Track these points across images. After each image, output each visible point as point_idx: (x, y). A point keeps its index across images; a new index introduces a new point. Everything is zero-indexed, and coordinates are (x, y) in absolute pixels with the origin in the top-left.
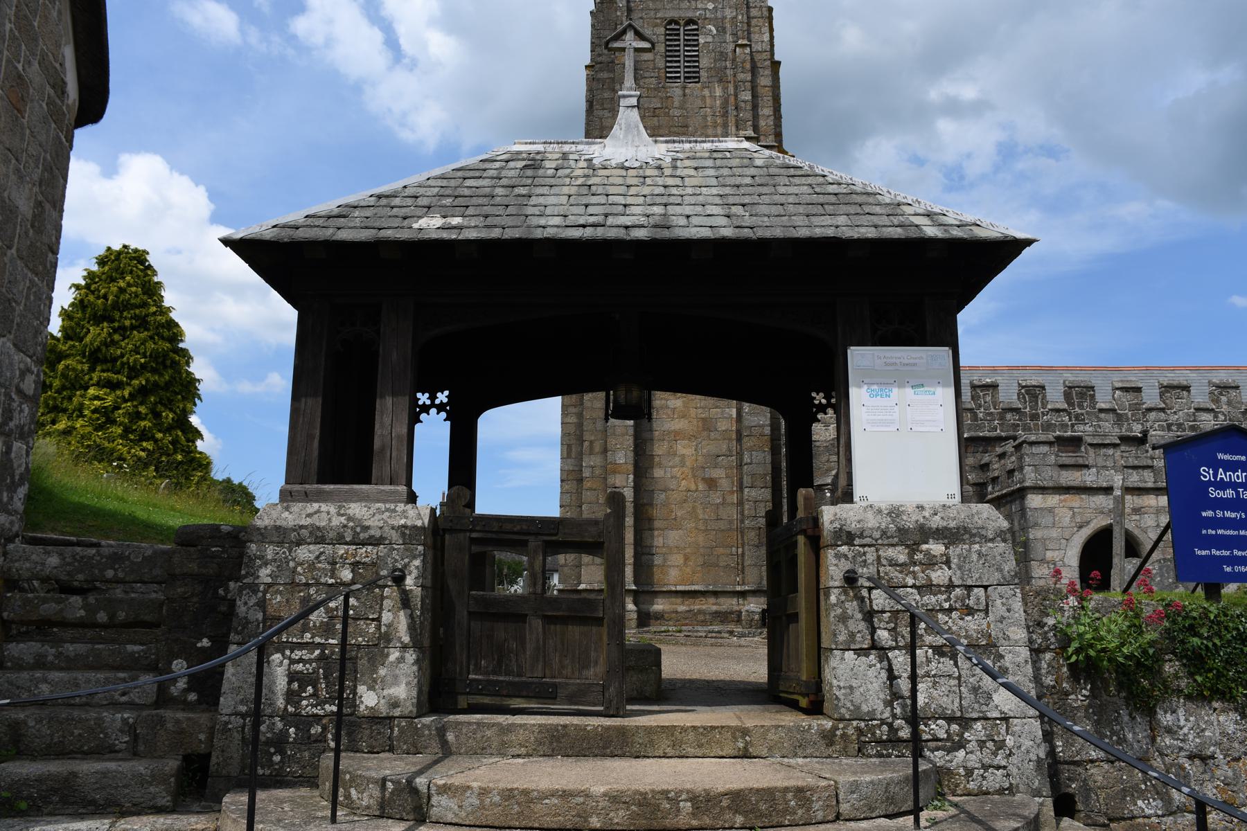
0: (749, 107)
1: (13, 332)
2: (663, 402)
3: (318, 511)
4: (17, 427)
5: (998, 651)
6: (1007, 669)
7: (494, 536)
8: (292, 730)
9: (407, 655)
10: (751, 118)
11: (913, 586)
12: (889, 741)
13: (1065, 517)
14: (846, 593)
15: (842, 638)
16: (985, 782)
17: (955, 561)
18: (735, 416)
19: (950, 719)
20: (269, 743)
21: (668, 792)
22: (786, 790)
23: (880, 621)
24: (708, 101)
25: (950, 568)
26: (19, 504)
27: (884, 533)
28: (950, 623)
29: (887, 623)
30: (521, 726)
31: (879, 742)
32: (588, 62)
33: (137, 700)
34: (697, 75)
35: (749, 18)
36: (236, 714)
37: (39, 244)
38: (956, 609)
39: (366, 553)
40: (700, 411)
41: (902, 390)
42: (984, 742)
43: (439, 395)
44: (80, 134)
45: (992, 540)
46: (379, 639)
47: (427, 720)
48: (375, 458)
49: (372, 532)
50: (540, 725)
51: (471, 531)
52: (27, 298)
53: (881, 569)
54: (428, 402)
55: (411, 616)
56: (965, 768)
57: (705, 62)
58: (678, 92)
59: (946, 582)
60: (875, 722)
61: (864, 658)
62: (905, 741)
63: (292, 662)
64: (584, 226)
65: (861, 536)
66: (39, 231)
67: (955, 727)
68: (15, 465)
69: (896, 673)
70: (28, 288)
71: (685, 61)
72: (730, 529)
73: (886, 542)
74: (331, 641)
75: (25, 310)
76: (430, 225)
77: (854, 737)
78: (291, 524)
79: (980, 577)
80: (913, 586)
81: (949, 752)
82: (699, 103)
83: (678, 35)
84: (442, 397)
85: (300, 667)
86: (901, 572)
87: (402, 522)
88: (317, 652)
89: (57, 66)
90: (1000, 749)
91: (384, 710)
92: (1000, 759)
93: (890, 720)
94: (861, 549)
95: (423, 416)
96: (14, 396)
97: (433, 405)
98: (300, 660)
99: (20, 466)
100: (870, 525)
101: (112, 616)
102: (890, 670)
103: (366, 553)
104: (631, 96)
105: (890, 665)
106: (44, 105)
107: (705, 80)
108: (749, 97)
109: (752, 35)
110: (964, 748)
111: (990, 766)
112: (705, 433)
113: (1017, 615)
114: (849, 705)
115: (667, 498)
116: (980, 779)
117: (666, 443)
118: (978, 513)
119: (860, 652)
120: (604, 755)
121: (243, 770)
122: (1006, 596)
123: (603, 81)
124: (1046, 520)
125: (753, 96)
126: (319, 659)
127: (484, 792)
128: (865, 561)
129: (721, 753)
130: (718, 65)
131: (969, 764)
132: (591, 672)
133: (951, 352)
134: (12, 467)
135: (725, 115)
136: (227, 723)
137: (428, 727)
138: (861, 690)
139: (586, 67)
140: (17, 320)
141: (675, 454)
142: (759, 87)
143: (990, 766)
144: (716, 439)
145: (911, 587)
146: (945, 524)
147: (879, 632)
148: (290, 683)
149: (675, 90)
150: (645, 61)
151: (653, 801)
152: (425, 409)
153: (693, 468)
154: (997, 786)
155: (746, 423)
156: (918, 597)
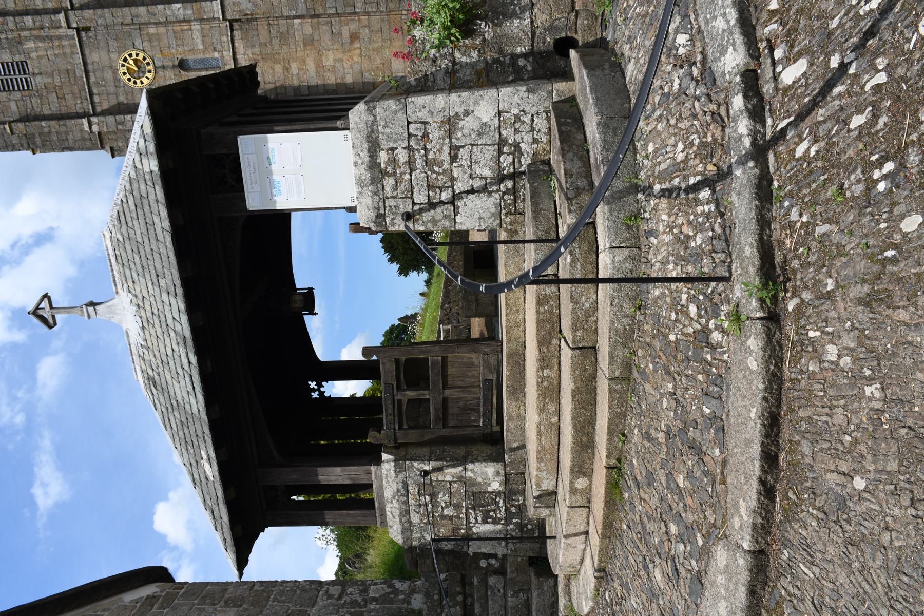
0: (39, 18)
1: (306, 609)
2: (294, 78)
3: (391, 512)
4: (361, 596)
5: (453, 117)
6: (465, 110)
7: (396, 418)
8: (514, 521)
9: (469, 468)
10: (48, 16)
11: (410, 174)
12: (514, 194)
14: (417, 220)
15: (447, 224)
16: (542, 130)
17: (391, 145)
18: (299, 20)
19: (500, 153)
20: (521, 530)
21: (538, 382)
22: (538, 312)
23: (435, 198)
24: (41, 53)
25: (396, 148)
26: (405, 585)
27: (375, 194)
28: (435, 150)
29: (436, 193)
30: (507, 410)
31: (515, 201)
32: (29, 153)
33: (502, 585)
36: (506, 546)
37: (251, 599)
38: (425, 145)
39: (413, 490)
40: (298, 48)
41: (274, 172)
42: (515, 129)
43: (311, 387)
44: (177, 580)
45: (375, 117)
46: (461, 482)
47: (506, 457)
48: (357, 482)
49: (400, 487)
50: (507, 400)
51: (394, 429)
52: (284, 602)
53: (400, 196)
54: (317, 393)
55: (447, 466)
56: (532, 144)
58: (38, 79)
59: (406, 151)
60: (502, 204)
61: (460, 210)
62: (515, 184)
63: (477, 522)
64: (194, 388)
65: (378, 209)
66: (243, 600)
67: (505, 149)
68: (383, 592)
69: (470, 188)
70: (278, 602)
71: (10, 74)
72: (388, 21)
73: (381, 192)
74: (464, 504)
75: (291, 602)
77: (512, 217)
78: (399, 526)
79: (402, 127)
80: (410, 174)
81: (522, 154)
82: (44, 61)
84: (313, 385)
85: (479, 519)
86: (401, 183)
87: (393, 472)
88: (470, 511)
89: (138, 605)
90: (520, 119)
91: (502, 478)
92: (527, 119)
93: (501, 193)
94: (387, 209)
95: (327, 395)
96: (343, 602)
97: (319, 390)
98: (476, 518)
99: (383, 589)
100: (371, 203)
101: (459, 593)
102: (468, 192)
103: (413, 490)
104: (87, 311)
105: (464, 192)
106: (166, 611)
107: (23, 56)
110: (519, 144)
111: (532, 126)
112: (316, 43)
113: (427, 101)
114: (491, 220)
115: (368, 71)
116: (540, 134)
117: (326, 74)
118: (356, 124)
119: (456, 212)
120: (524, 365)
121: (537, 542)
122: (414, 108)
126: (474, 508)
127: (539, 470)
128: (395, 206)
129: (522, 299)
131: (530, 140)
132: (476, 361)
133: (241, 136)
134: (384, 595)
135: (50, 38)
136: (511, 550)
137: (510, 456)
138: (481, 212)
139: (34, 154)
140: (298, 608)
141: (334, 67)
142: (18, 8)
143: (532, 126)
144: (319, 35)
145: (411, 176)
146: (366, 151)
147: (442, 199)
148: (488, 523)
150: (18, 108)
151: (543, 391)
152: (322, 394)
153: (344, 52)
154: (545, 121)
155: (304, 13)
156: (418, 172)
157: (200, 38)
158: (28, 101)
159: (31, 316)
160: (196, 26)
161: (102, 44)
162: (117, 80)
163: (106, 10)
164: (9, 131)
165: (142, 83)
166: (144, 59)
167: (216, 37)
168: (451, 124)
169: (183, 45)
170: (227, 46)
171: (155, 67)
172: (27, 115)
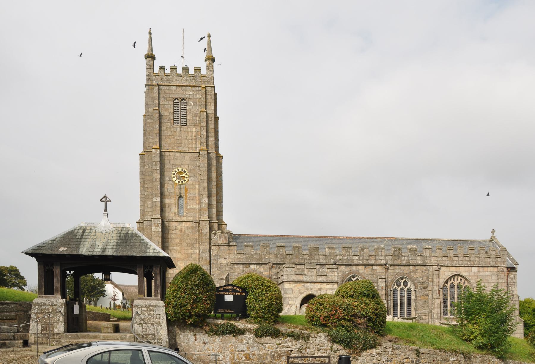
0: (205, 137)
10: (206, 142)
13: (296, 290)
18: (198, 253)
24: (190, 133)
32: (144, 114)
34: (186, 122)
35: (206, 99)
40: (186, 251)
43: (71, 272)
54: (69, 273)
57: (189, 117)
58: (178, 129)
65: (139, 306)
76: (62, 250)
83: (179, 105)
92: (160, 341)
108: (205, 133)
109: (207, 106)
119: (138, 324)
123: (149, 123)
124: (290, 292)
125: (206, 132)
130: (194, 119)
148: (42, 328)
149: (177, 128)
155: (201, 256)
157: (193, 207)
158: (168, 122)
159: (104, 195)
160: (198, 207)
161: (192, 162)
162: (176, 166)
163: (206, 169)
164: (155, 109)
165: (174, 177)
166: (185, 181)
167: (192, 215)
168: (159, 324)
169: (190, 199)
170: (188, 219)
171: (181, 184)
172: (161, 119)
